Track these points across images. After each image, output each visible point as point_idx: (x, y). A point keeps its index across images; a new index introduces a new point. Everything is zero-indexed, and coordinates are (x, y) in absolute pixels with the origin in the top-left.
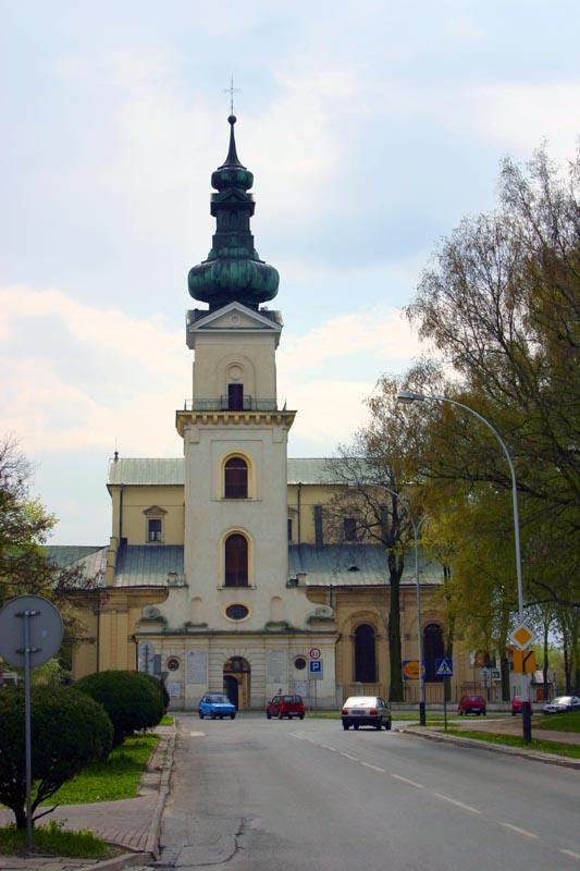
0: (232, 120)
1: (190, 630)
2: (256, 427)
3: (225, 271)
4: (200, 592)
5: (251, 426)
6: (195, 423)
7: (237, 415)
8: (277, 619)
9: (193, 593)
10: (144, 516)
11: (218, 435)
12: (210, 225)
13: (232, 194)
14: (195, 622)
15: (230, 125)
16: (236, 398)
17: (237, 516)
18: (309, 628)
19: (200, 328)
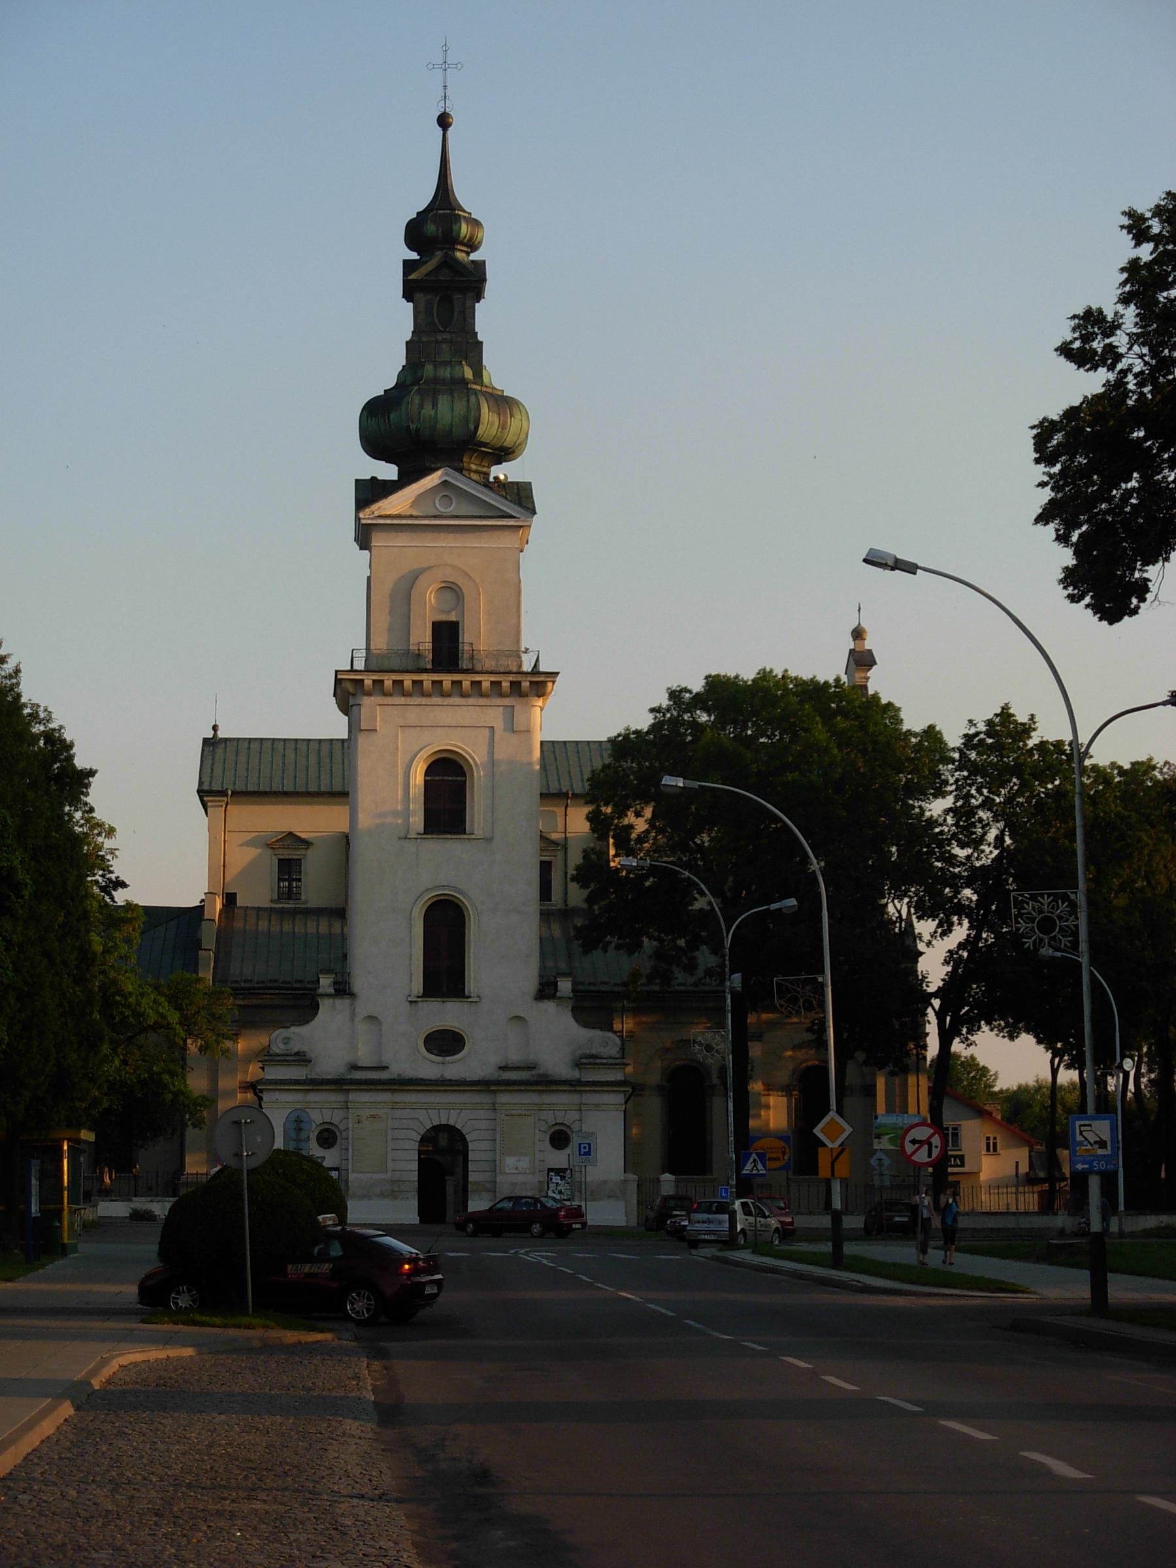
0: (444, 121)
1: (358, 1075)
2: (482, 701)
5: (471, 701)
6: (369, 694)
7: (447, 679)
8: (515, 1057)
9: (364, 1006)
12: (401, 319)
13: (442, 266)
15: (440, 131)
16: (447, 635)
17: (445, 865)
18: (576, 1074)
19: (380, 517)
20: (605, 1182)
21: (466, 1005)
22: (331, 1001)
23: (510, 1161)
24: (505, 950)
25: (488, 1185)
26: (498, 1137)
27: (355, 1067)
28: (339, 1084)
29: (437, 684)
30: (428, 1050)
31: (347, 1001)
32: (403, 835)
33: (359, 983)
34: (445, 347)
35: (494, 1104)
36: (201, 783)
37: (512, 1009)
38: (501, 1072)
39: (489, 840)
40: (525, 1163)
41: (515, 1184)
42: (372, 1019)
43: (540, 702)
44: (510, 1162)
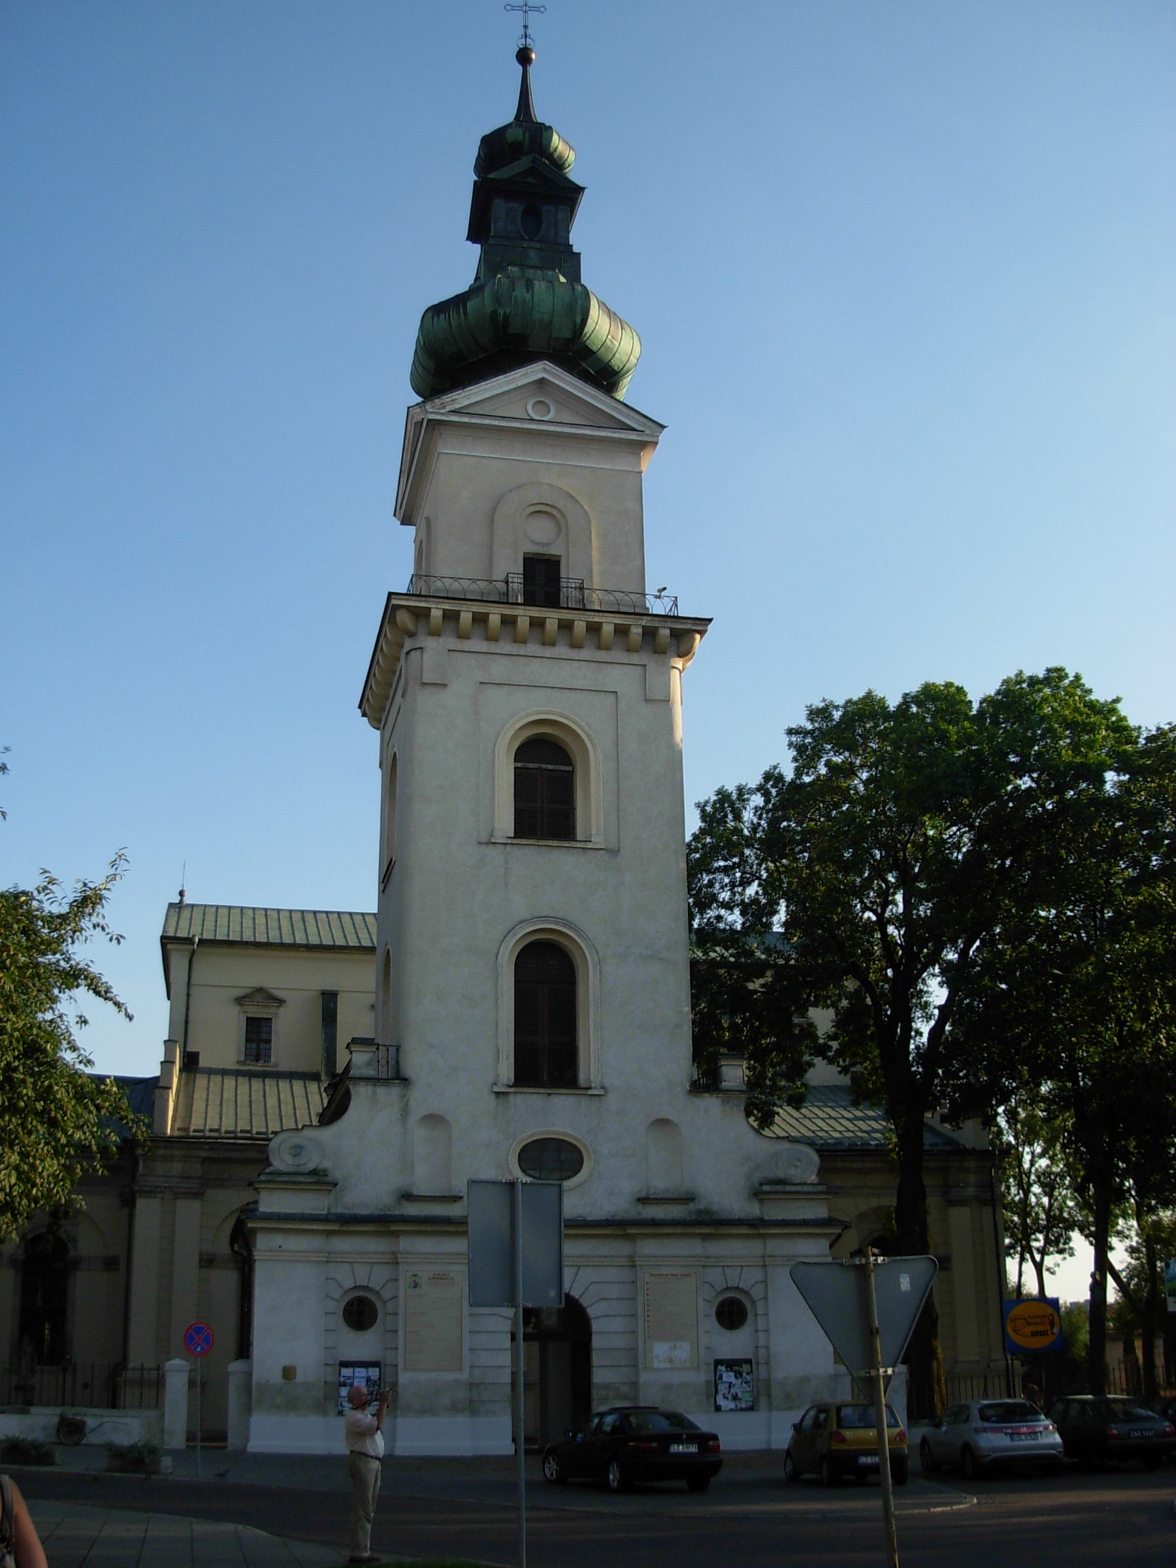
0: (524, 57)
1: (411, 1209)
2: (601, 655)
3: (520, 292)
4: (454, 1109)
5: (586, 654)
6: (435, 633)
7: (524, 615)
8: (660, 1184)
9: (422, 1100)
10: (236, 1009)
11: (499, 669)
13: (522, 190)
14: (421, 1189)
15: (519, 68)
16: (543, 578)
18: (754, 1210)
19: (454, 412)
20: (805, 1380)
21: (584, 1101)
22: (370, 1089)
23: (660, 1349)
24: (636, 1021)
25: (625, 1389)
26: (640, 1310)
27: (407, 1196)
28: (382, 1223)
29: (537, 624)
30: (524, 1171)
31: (396, 1090)
32: (484, 839)
33: (415, 1062)
34: (532, 253)
35: (631, 1258)
36: (164, 930)
37: (648, 1105)
38: (640, 1206)
39: (614, 852)
40: (683, 1351)
41: (668, 1387)
42: (434, 1120)
43: (678, 663)
44: (655, 1356)
